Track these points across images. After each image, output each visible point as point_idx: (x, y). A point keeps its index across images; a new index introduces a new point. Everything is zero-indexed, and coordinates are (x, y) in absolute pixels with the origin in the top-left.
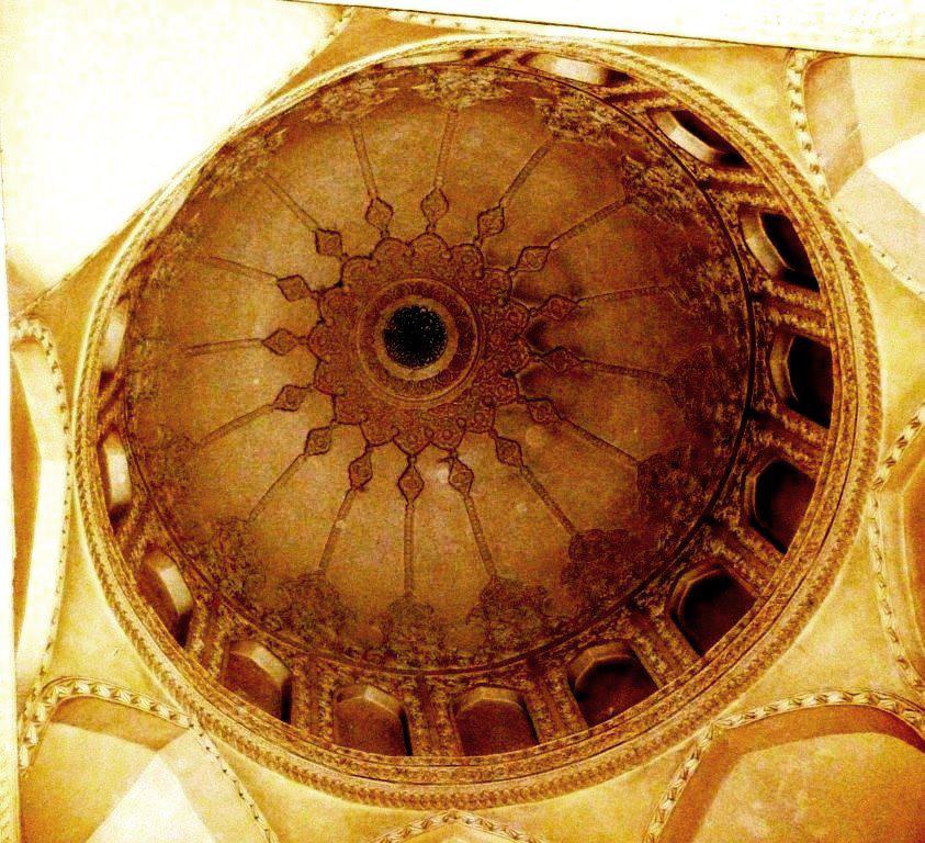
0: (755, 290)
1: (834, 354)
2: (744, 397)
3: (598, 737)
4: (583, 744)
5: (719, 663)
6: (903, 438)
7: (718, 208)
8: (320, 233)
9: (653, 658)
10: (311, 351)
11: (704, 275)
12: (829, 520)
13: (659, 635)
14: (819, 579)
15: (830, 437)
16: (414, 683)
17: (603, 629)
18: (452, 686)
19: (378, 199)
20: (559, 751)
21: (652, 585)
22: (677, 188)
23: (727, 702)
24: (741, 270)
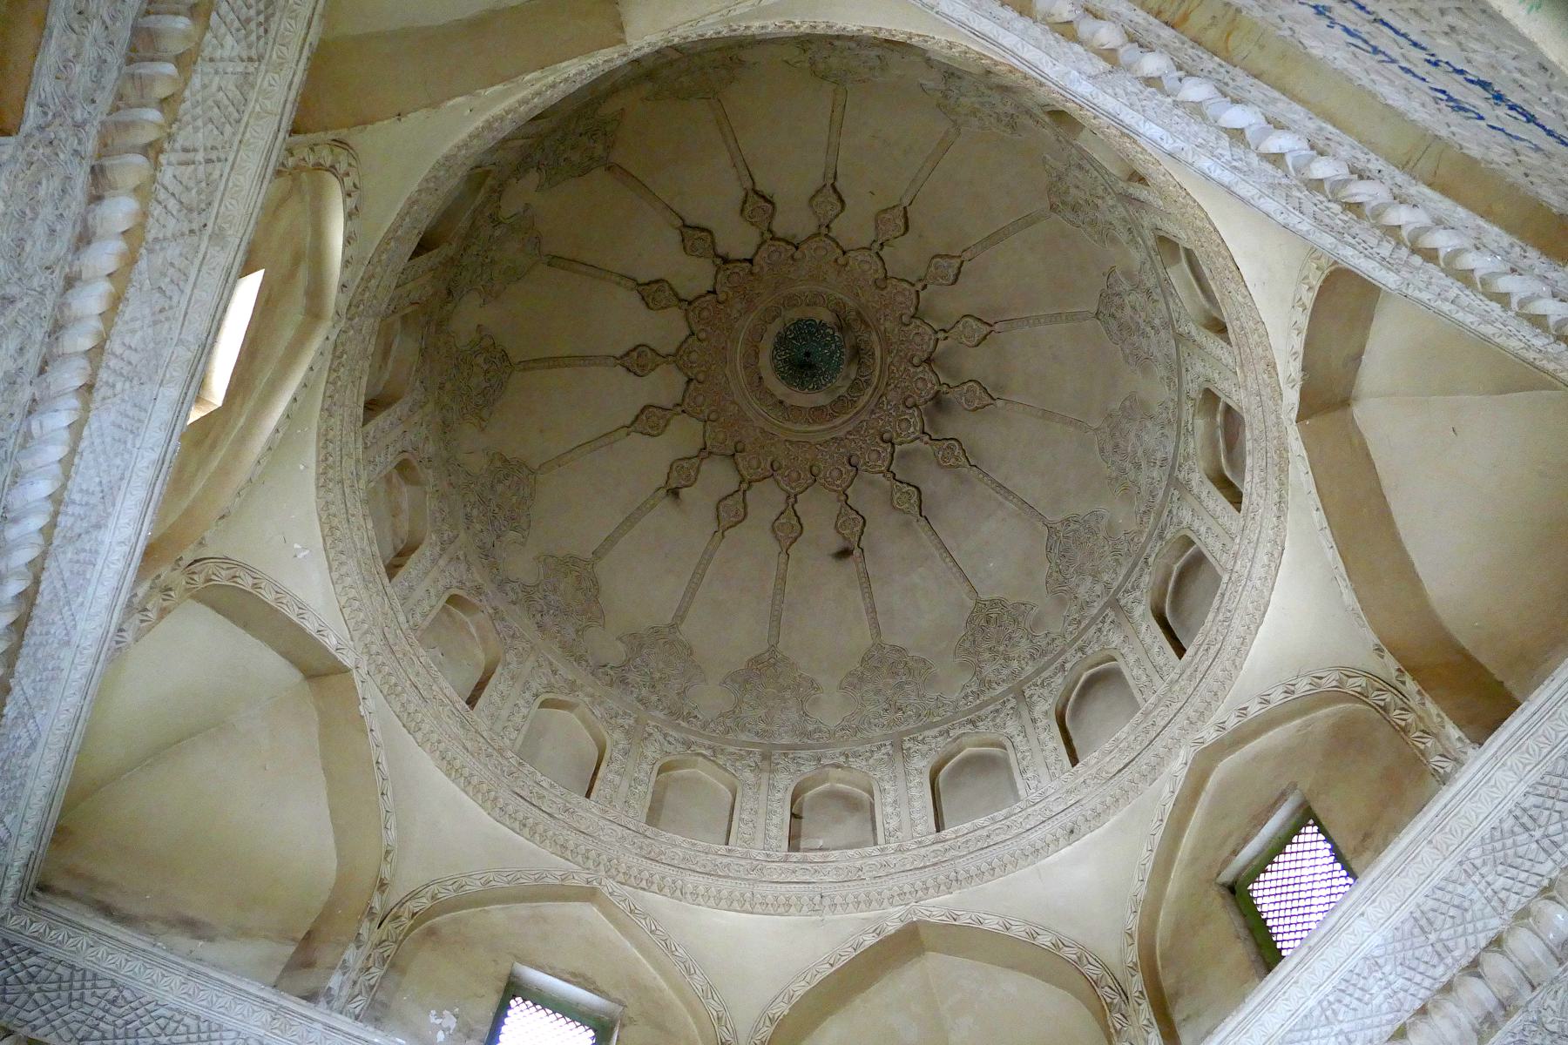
0: (1181, 477)
1: (1223, 586)
2: (1115, 585)
3: (792, 866)
4: (774, 865)
5: (951, 848)
6: (1245, 709)
7: (1184, 370)
8: (751, 194)
9: (889, 810)
10: (687, 319)
11: (1138, 436)
12: (1133, 755)
13: (908, 788)
14: (1093, 810)
15: (1177, 670)
16: (632, 722)
17: (857, 755)
18: (670, 743)
19: (833, 186)
20: (743, 862)
21: (927, 733)
22: (1153, 328)
23: (938, 892)
24: (1177, 447)
